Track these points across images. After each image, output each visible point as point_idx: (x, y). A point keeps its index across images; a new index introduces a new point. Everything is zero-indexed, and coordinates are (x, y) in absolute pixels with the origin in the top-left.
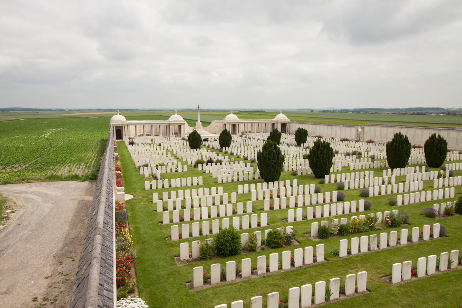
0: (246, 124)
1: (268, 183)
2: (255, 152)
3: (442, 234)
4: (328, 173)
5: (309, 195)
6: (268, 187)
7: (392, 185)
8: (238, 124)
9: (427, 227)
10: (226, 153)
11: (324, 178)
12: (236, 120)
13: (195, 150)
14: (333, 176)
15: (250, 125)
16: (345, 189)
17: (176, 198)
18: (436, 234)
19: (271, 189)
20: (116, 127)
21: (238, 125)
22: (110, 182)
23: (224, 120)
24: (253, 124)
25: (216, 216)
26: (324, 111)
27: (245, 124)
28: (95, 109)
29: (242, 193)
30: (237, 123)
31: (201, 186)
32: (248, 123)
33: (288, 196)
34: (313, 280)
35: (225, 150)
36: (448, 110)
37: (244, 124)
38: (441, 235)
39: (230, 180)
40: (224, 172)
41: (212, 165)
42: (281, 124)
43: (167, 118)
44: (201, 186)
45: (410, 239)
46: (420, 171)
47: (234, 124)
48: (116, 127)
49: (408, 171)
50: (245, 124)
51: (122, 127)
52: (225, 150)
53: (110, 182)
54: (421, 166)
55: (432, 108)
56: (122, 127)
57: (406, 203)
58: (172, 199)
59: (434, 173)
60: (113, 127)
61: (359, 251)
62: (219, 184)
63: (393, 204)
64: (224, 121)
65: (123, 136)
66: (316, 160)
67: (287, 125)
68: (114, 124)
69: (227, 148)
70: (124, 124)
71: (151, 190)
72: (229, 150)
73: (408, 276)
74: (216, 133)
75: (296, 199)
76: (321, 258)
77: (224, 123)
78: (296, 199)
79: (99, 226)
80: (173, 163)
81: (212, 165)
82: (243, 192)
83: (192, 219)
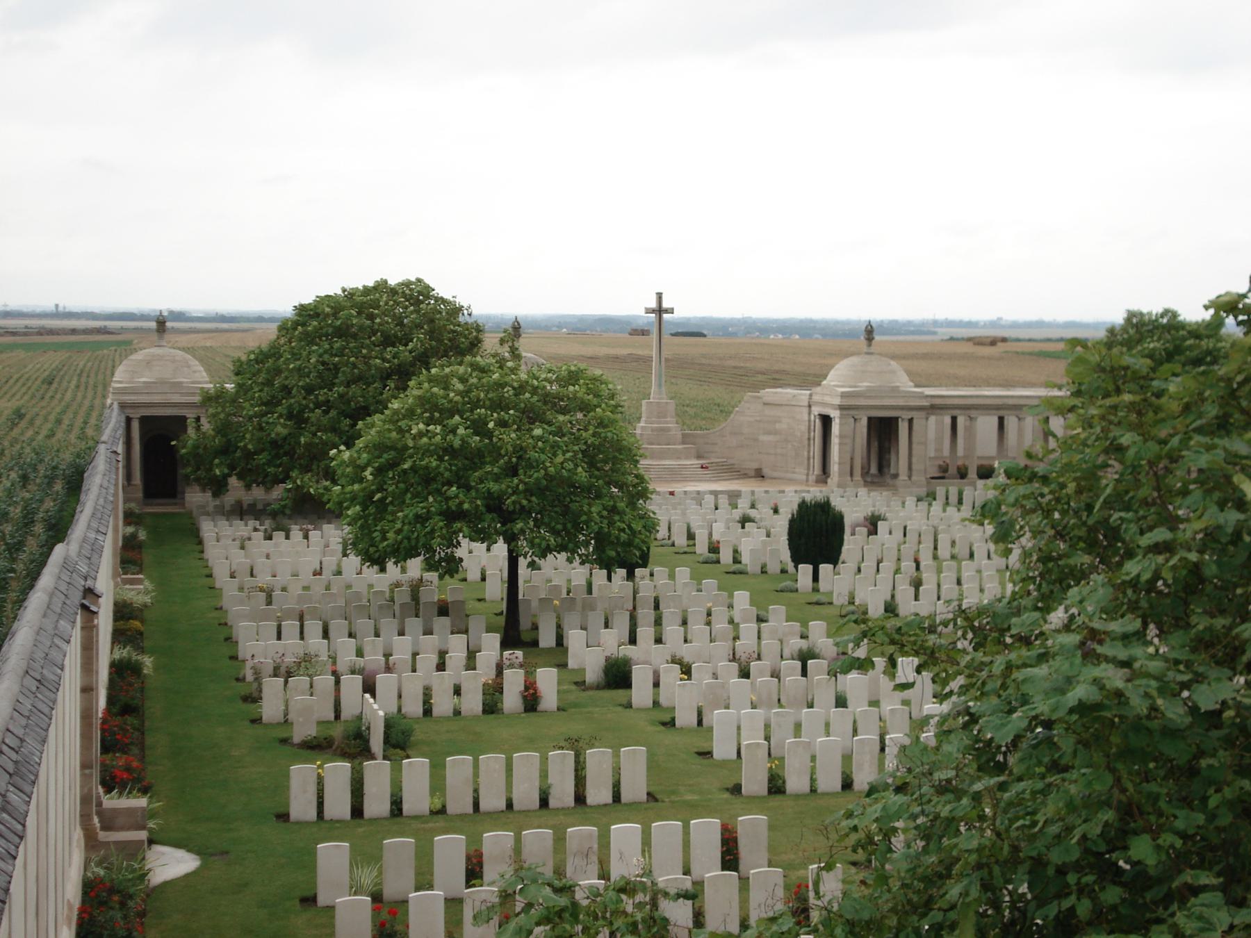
0: (961, 421)
8: (906, 415)
10: (819, 603)
12: (895, 389)
15: (987, 424)
17: (412, 884)
21: (911, 421)
22: (16, 762)
23: (818, 389)
24: (1011, 422)
27: (954, 419)
28: (38, 310)
30: (902, 408)
31: (633, 805)
32: (973, 413)
35: (816, 578)
37: (948, 420)
39: (830, 781)
40: (700, 754)
42: (136, 426)
43: (812, 379)
47: (882, 420)
48: (144, 420)
50: (954, 419)
53: (16, 762)
60: (129, 420)
62: (752, 798)
64: (815, 398)
66: (990, 873)
68: (135, 406)
74: (766, 471)
77: (816, 410)
79: (1070, 695)
80: (442, 654)
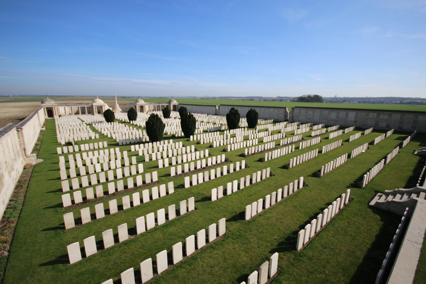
1: (152, 143)
2: (82, 130)
3: (246, 166)
4: (193, 134)
5: (171, 150)
6: (160, 144)
7: (94, 165)
9: (238, 164)
10: (133, 124)
11: (190, 137)
13: (110, 123)
14: (195, 136)
16: (201, 144)
18: (243, 167)
19: (169, 144)
20: (46, 108)
25: (185, 153)
26: (202, 98)
29: (134, 150)
33: (94, 164)
34: (144, 214)
35: (133, 122)
36: (265, 98)
38: (246, 167)
41: (85, 138)
42: (45, 109)
44: (106, 148)
45: (228, 172)
46: (244, 131)
48: (46, 108)
49: (237, 131)
51: (52, 108)
52: (133, 122)
54: (244, 128)
55: (399, 97)
56: (52, 108)
57: (233, 149)
58: (206, 138)
59: (251, 131)
61: (198, 183)
63: (225, 150)
65: (54, 115)
67: (54, 108)
69: (134, 121)
70: (53, 106)
71: (74, 152)
72: (134, 122)
73: (221, 195)
75: (220, 142)
76: (171, 191)
78: (220, 142)
81: (85, 138)
82: (135, 150)
83: (178, 154)
